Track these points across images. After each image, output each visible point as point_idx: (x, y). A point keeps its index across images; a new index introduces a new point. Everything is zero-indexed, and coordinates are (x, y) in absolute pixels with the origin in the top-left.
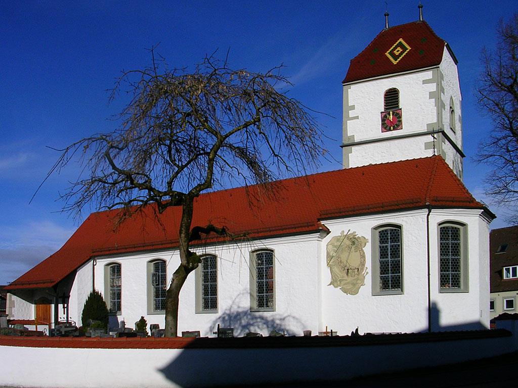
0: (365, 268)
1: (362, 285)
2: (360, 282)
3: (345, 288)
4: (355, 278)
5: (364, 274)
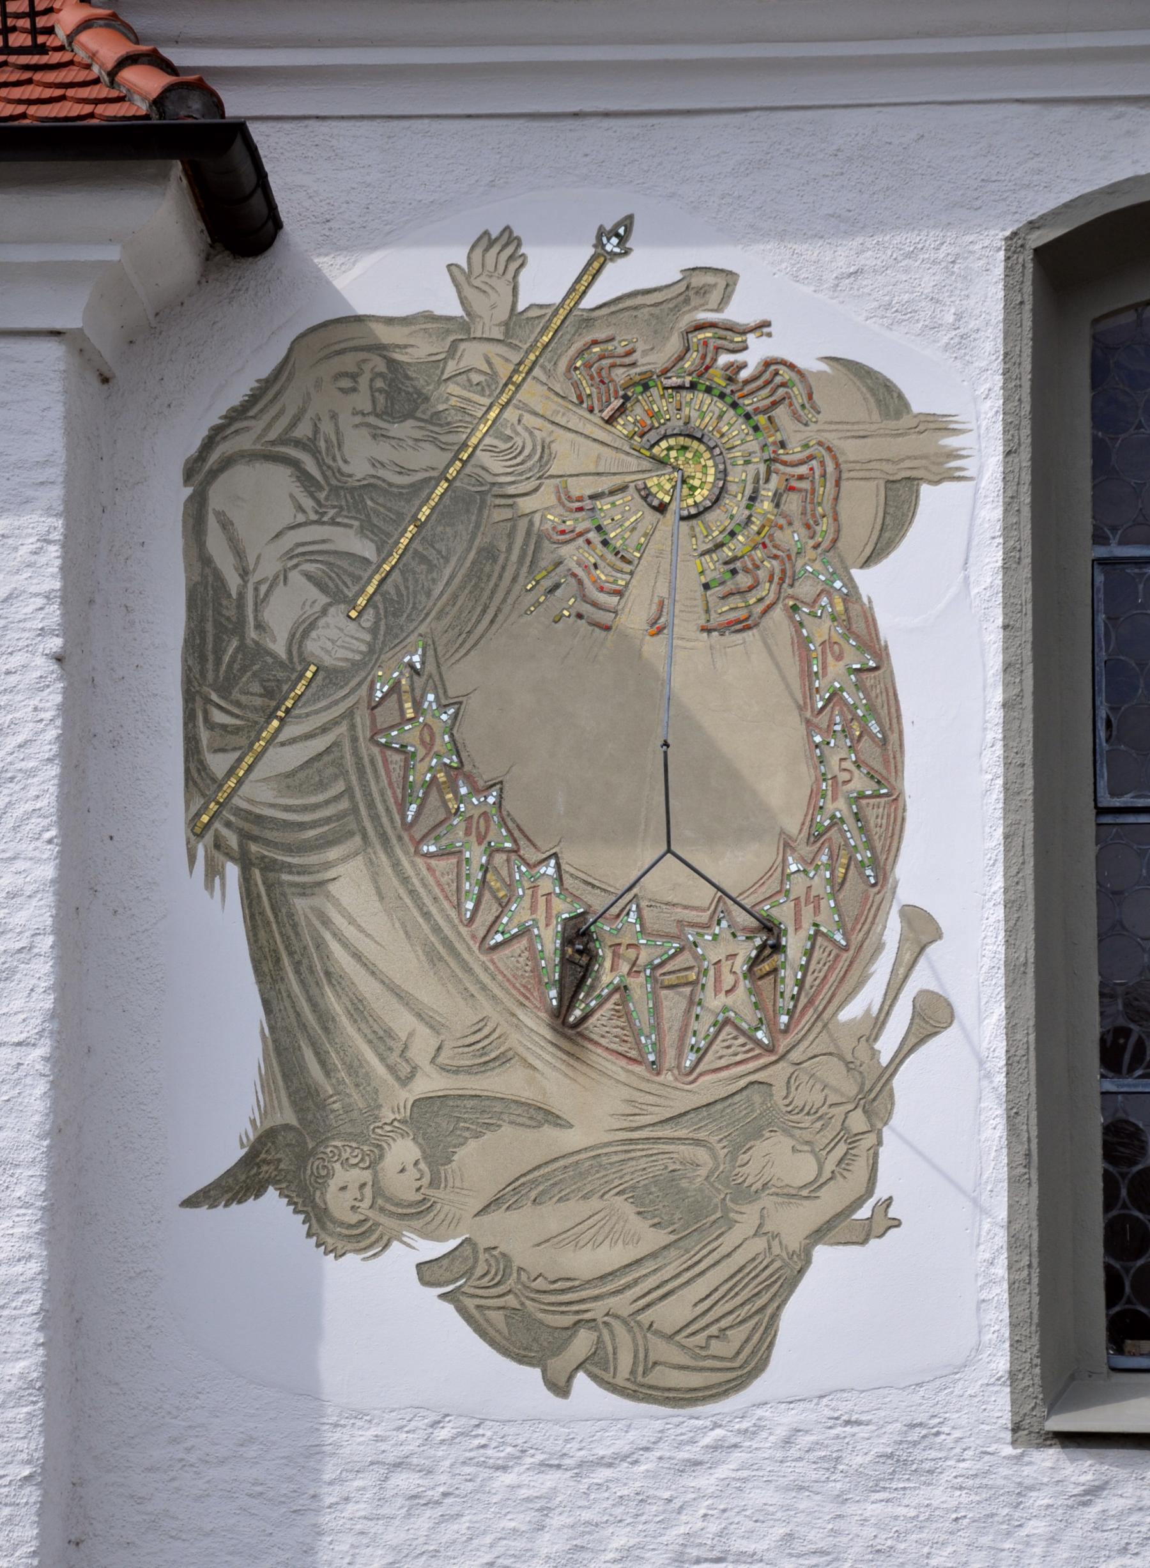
0: (892, 930)
1: (819, 1234)
2: (804, 1169)
3: (522, 1253)
4: (709, 1088)
5: (879, 1022)
